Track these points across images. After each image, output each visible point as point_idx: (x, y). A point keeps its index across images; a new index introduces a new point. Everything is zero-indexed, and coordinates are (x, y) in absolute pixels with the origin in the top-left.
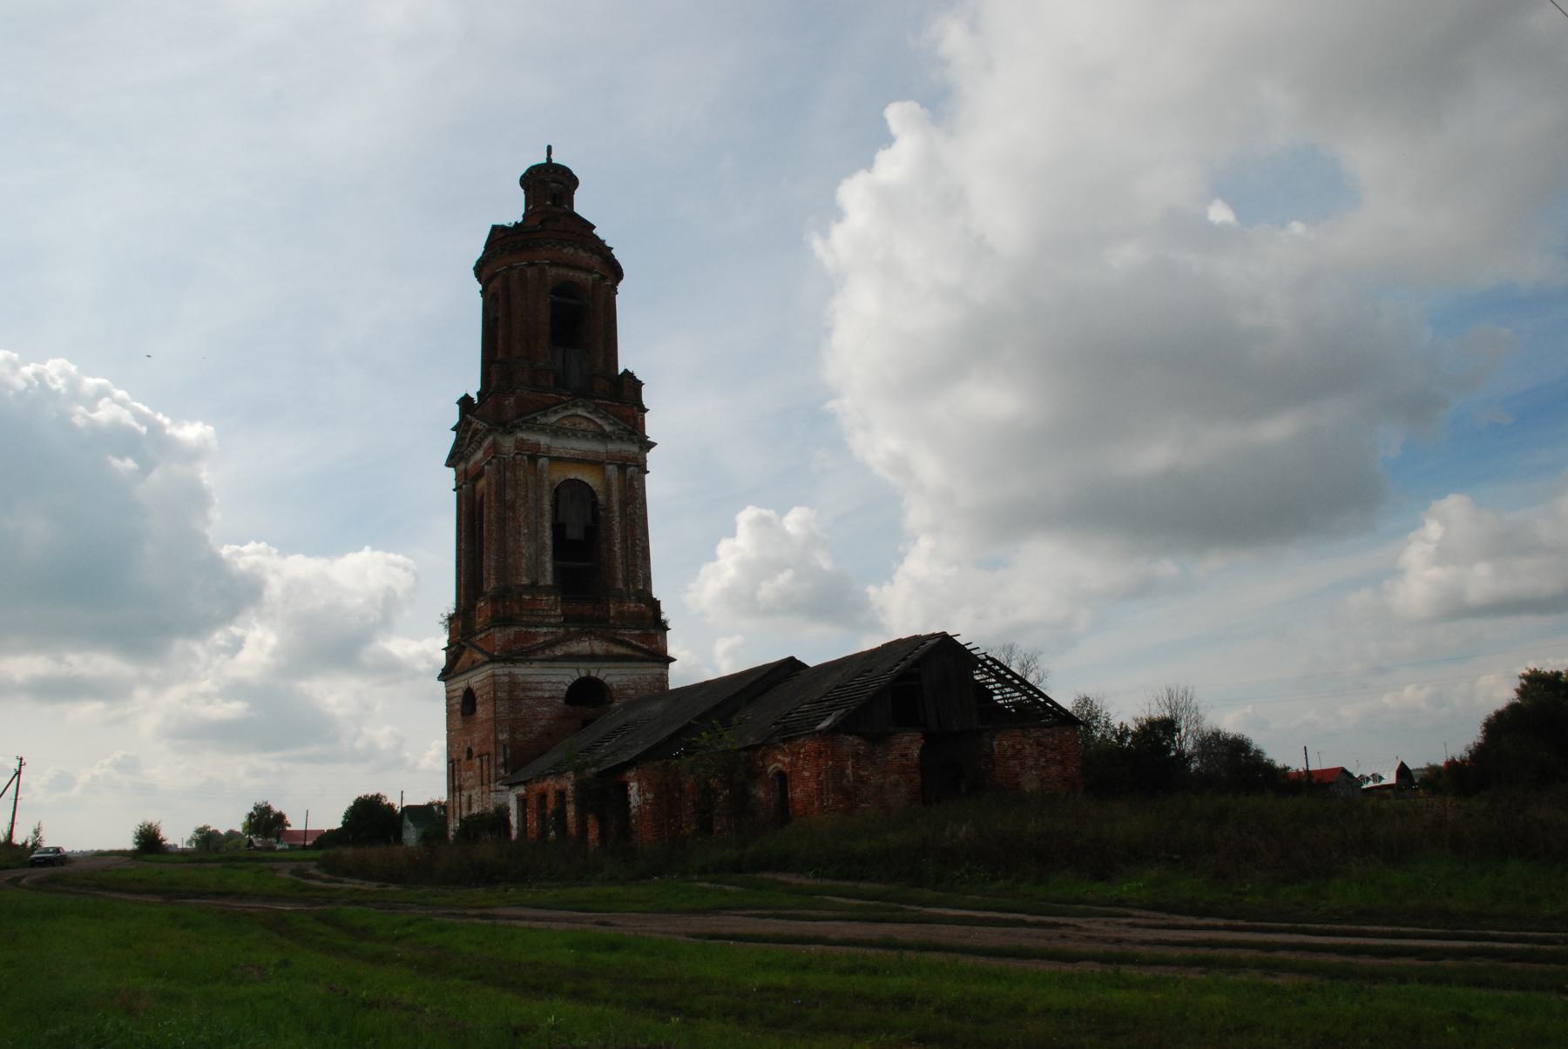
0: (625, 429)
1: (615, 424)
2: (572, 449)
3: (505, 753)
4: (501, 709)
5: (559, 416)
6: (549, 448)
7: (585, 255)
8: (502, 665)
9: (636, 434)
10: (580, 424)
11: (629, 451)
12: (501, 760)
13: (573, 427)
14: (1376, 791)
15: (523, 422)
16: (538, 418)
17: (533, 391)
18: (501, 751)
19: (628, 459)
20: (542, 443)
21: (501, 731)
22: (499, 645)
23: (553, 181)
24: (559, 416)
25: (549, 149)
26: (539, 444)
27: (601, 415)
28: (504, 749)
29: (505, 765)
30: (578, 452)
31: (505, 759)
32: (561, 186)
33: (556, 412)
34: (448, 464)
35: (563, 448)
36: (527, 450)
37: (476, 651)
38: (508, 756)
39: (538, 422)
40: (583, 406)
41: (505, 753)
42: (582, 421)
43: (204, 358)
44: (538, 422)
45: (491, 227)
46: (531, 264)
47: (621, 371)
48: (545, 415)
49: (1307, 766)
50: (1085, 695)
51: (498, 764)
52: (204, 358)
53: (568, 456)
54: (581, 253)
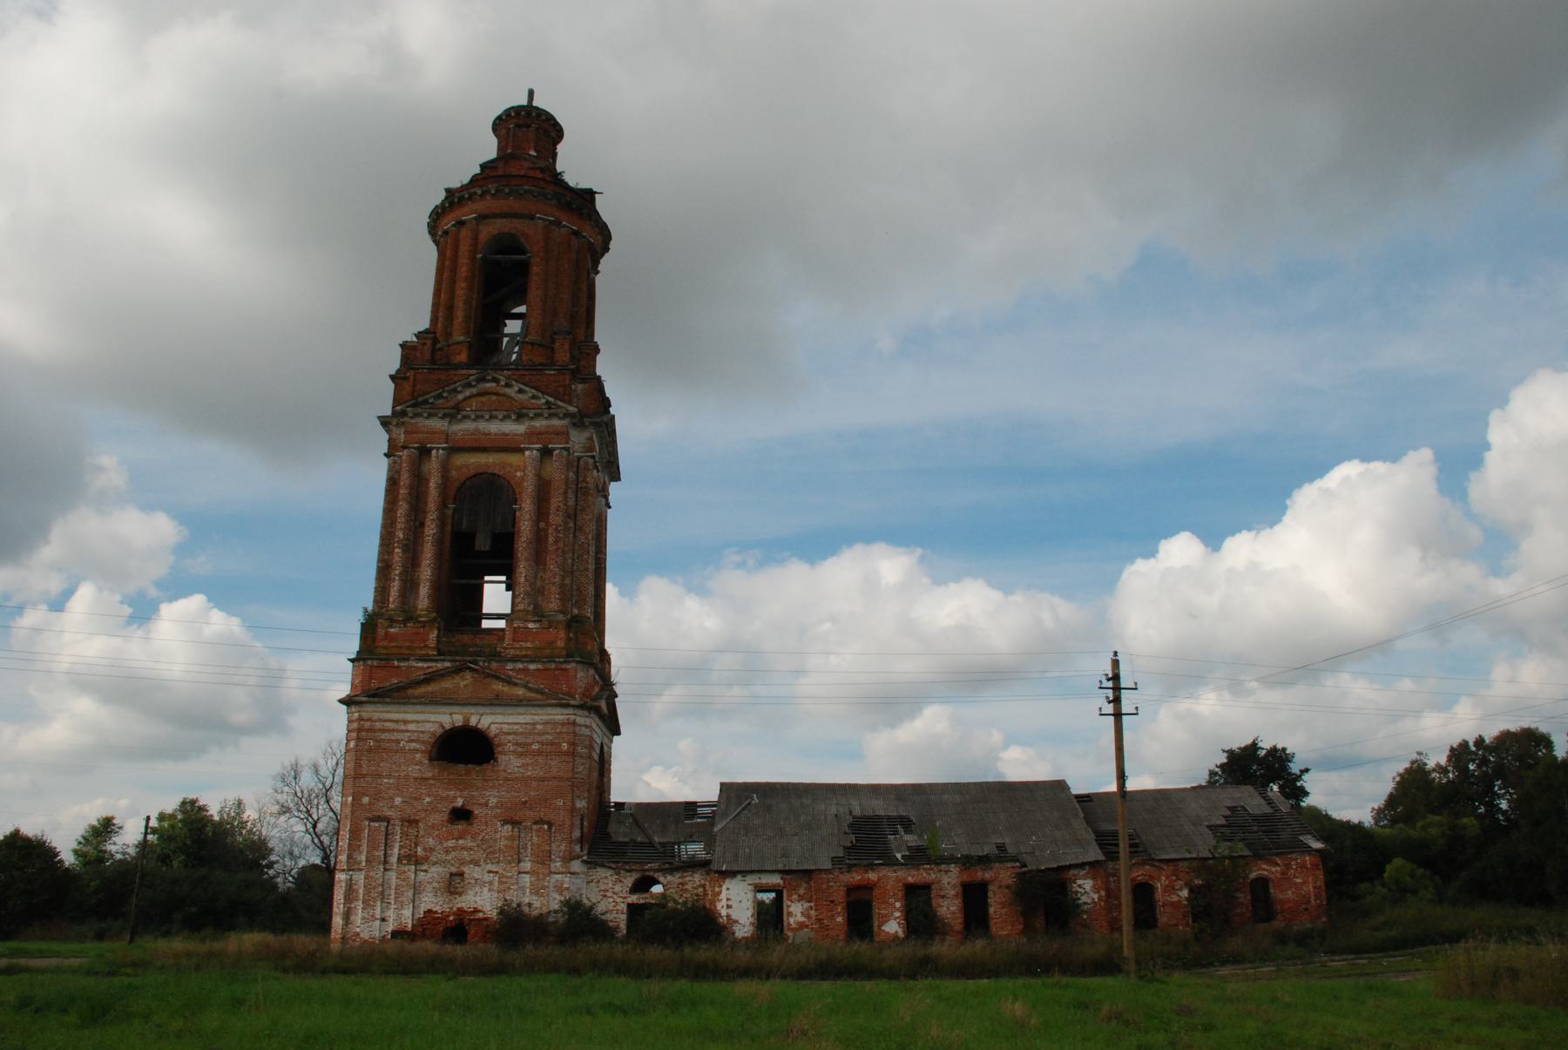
3: (582, 824)
4: (581, 768)
8: (586, 713)
12: (577, 834)
18: (578, 822)
21: (579, 797)
22: (581, 687)
28: (582, 820)
29: (581, 841)
31: (582, 833)
34: (614, 416)
37: (494, 681)
38: (585, 830)
41: (582, 824)
43: (887, 234)
49: (1121, 777)
50: (121, 834)
51: (574, 838)
52: (887, 234)
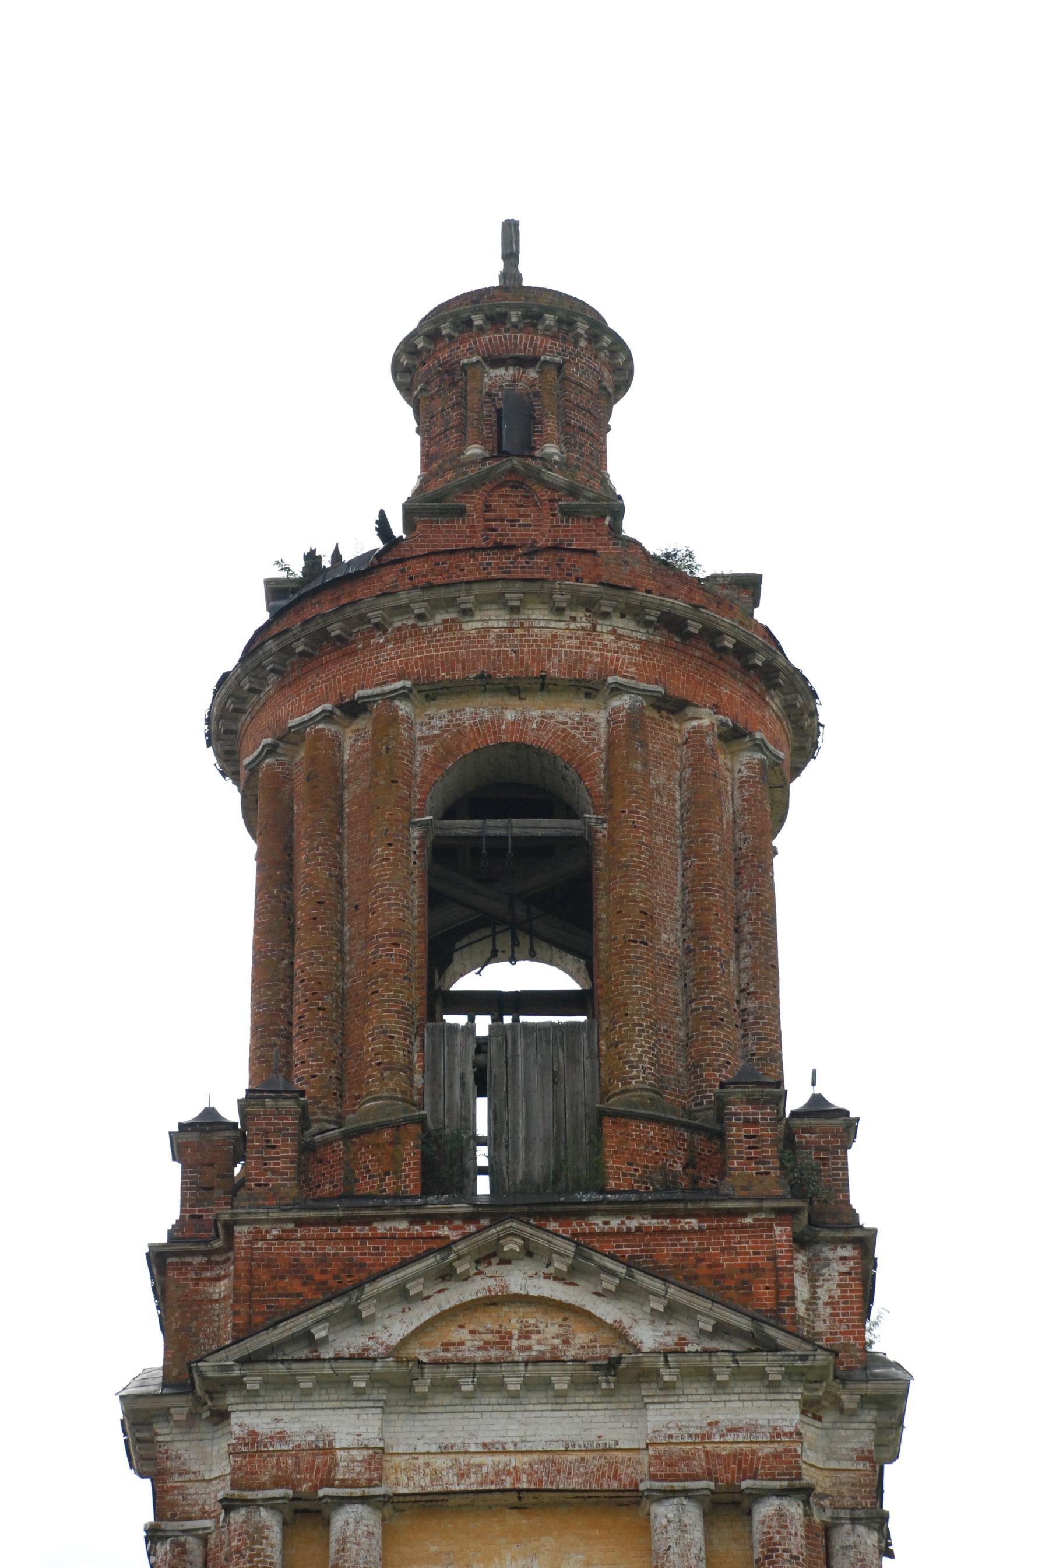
0: (721, 1330)
1: (671, 1311)
2: (488, 1449)
5: (422, 1314)
6: (378, 1456)
7: (558, 625)
9: (775, 1348)
10: (525, 1335)
11: (752, 1428)
13: (494, 1353)
14: (157, 1501)
15: (246, 1360)
16: (320, 1333)
17: (300, 1223)
19: (744, 1464)
20: (341, 1442)
23: (496, 362)
24: (422, 1314)
25: (511, 232)
26: (329, 1449)
27: (609, 1284)
30: (514, 1461)
32: (532, 374)
33: (402, 1295)
35: (444, 1451)
36: (276, 1484)
39: (327, 1353)
40: (528, 1252)
42: (534, 1318)
44: (327, 1353)
45: (758, 572)
46: (353, 709)
47: (796, 1099)
48: (355, 1317)
53: (470, 1483)
54: (538, 617)
